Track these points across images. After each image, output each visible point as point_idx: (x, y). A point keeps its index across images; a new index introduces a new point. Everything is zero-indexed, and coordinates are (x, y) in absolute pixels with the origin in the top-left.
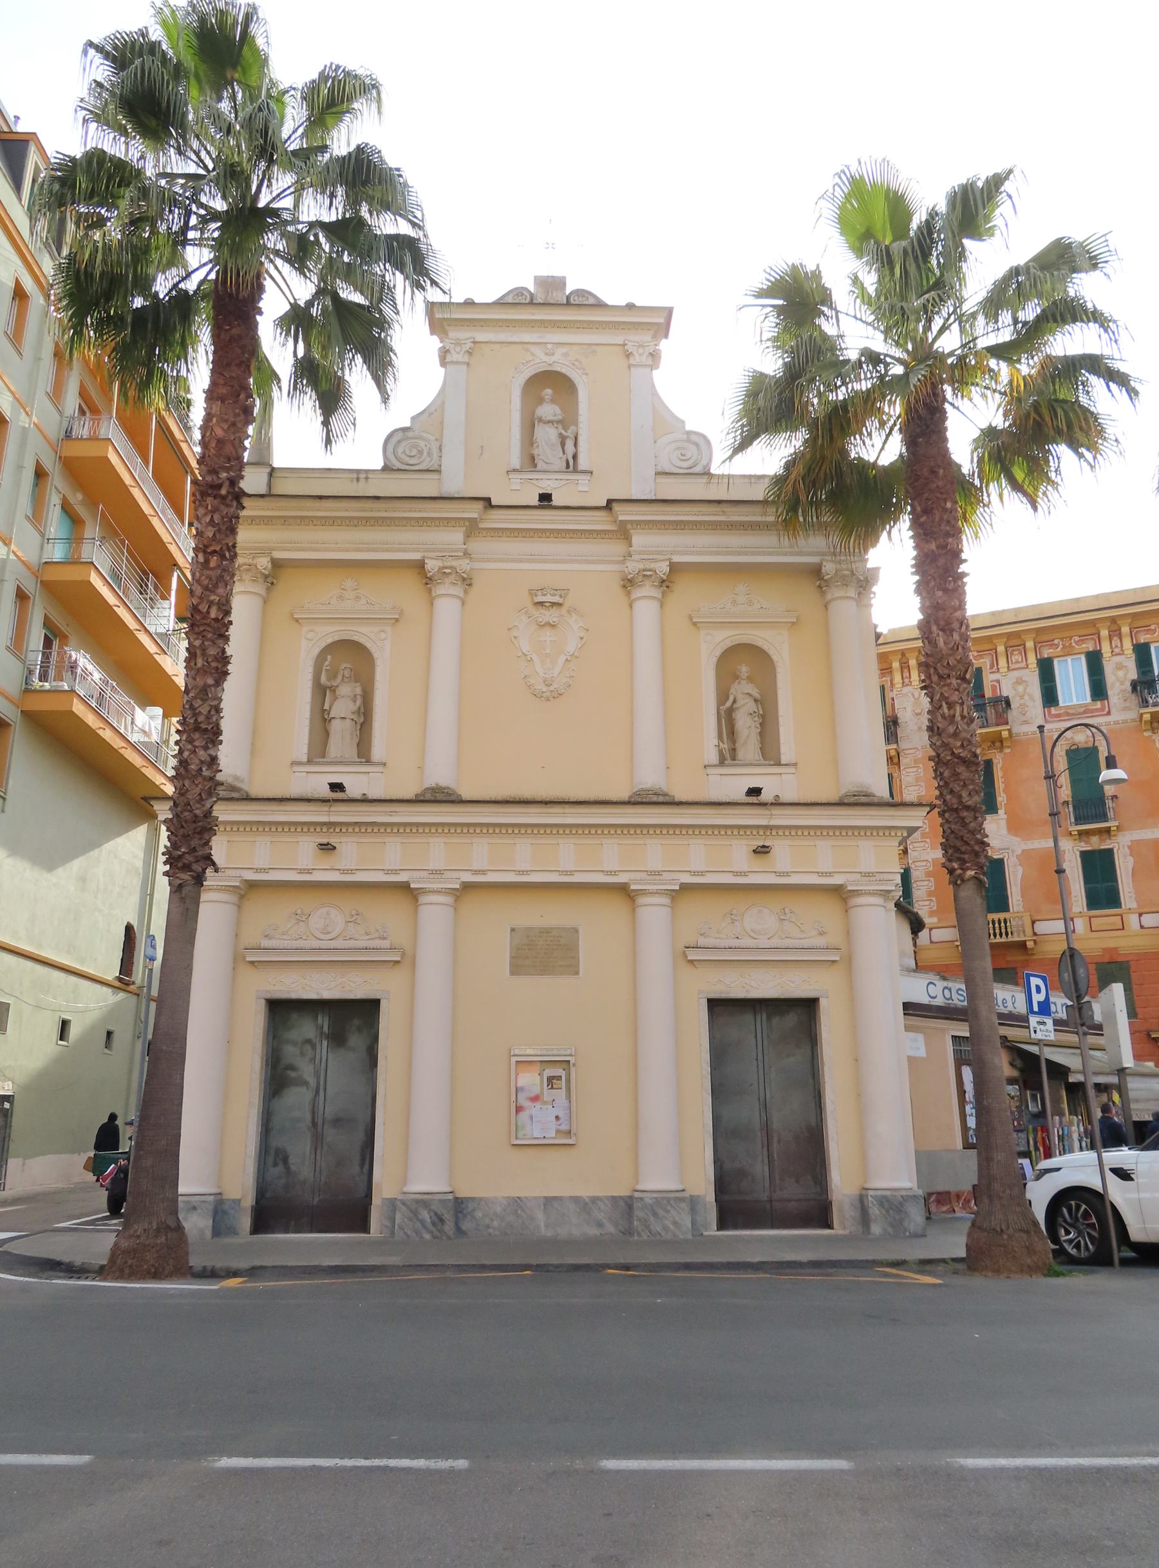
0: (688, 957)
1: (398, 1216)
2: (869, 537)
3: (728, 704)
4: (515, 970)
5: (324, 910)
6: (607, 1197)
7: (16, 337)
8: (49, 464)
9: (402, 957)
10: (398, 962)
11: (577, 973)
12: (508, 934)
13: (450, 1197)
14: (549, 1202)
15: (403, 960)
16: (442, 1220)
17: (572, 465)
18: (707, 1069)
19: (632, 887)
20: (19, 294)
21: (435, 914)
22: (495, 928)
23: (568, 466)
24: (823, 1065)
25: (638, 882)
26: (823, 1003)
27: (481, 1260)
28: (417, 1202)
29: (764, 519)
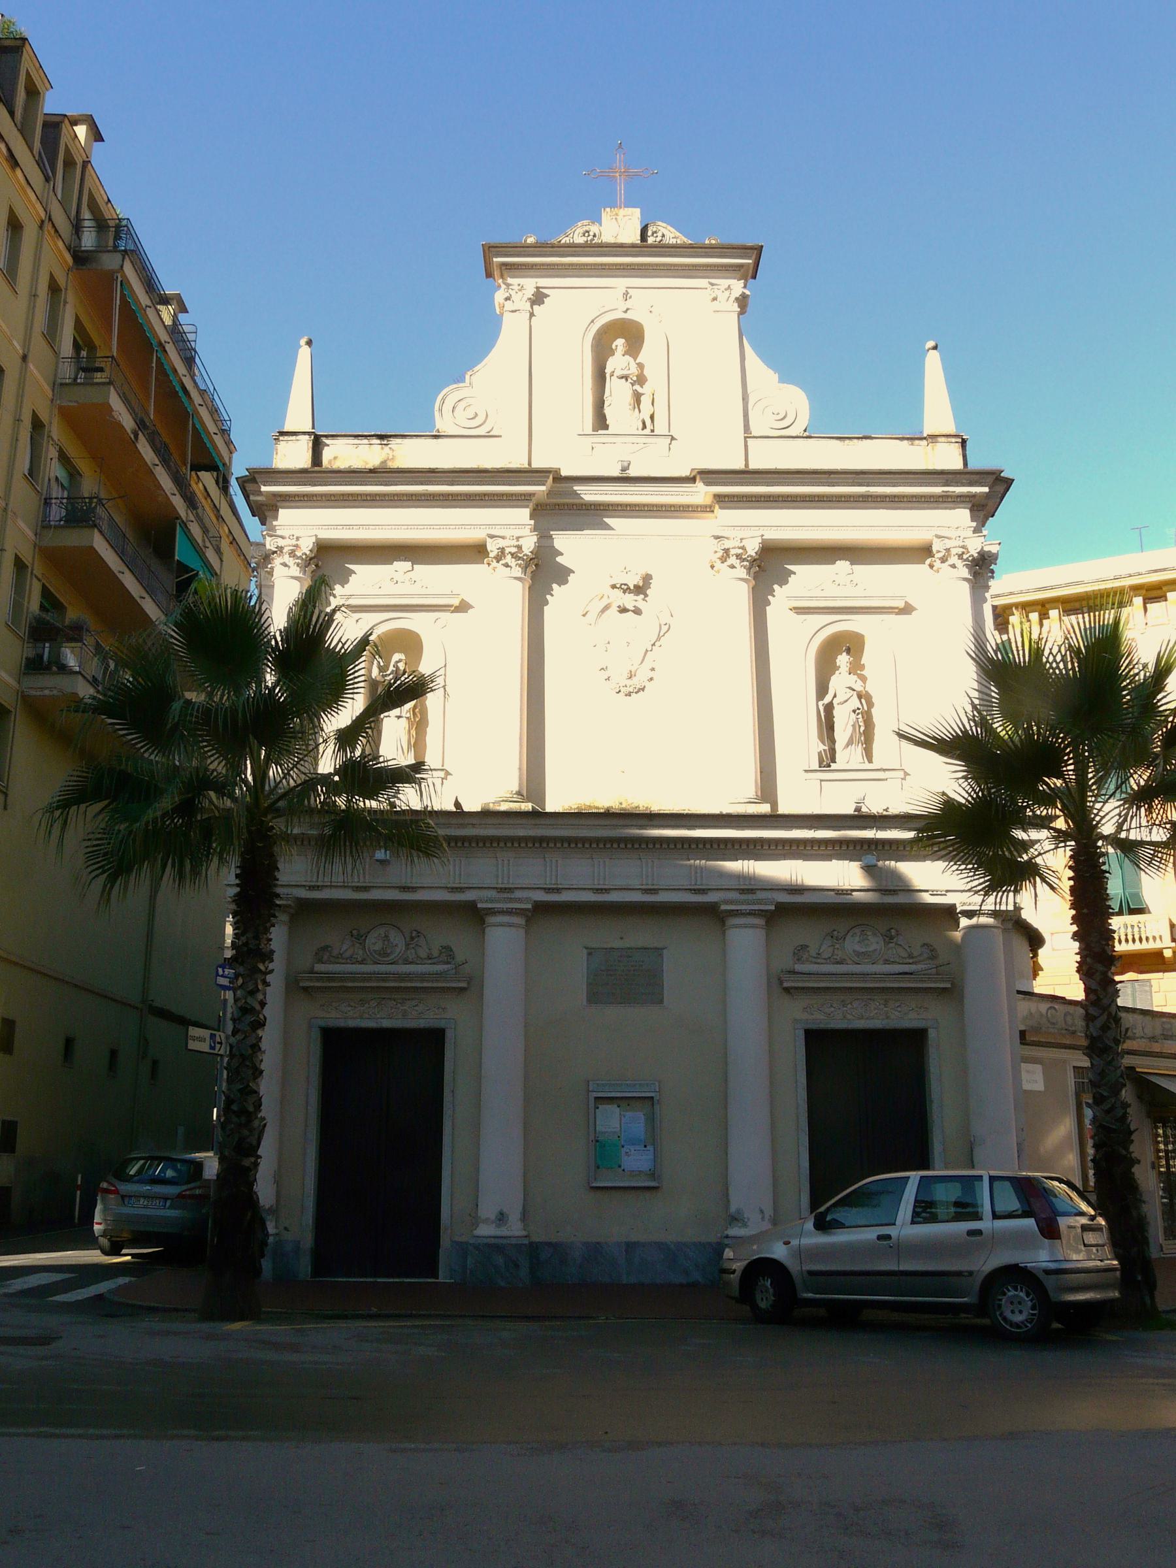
0: (785, 986)
1: (470, 1261)
2: (1094, 1097)
3: (827, 699)
4: (594, 997)
5: (381, 931)
6: (695, 1244)
7: (11, 272)
8: (27, 558)
9: (468, 983)
10: (462, 990)
11: (661, 1001)
12: (585, 958)
13: (526, 1241)
14: (631, 1247)
15: (468, 987)
16: (517, 1266)
17: (647, 426)
18: (803, 1094)
19: (723, 907)
20: (15, 225)
21: (503, 944)
22: (573, 952)
23: (644, 427)
24: (932, 1102)
25: (727, 902)
26: (932, 1034)
27: (560, 1295)
28: (489, 1245)
29: (978, 1321)
